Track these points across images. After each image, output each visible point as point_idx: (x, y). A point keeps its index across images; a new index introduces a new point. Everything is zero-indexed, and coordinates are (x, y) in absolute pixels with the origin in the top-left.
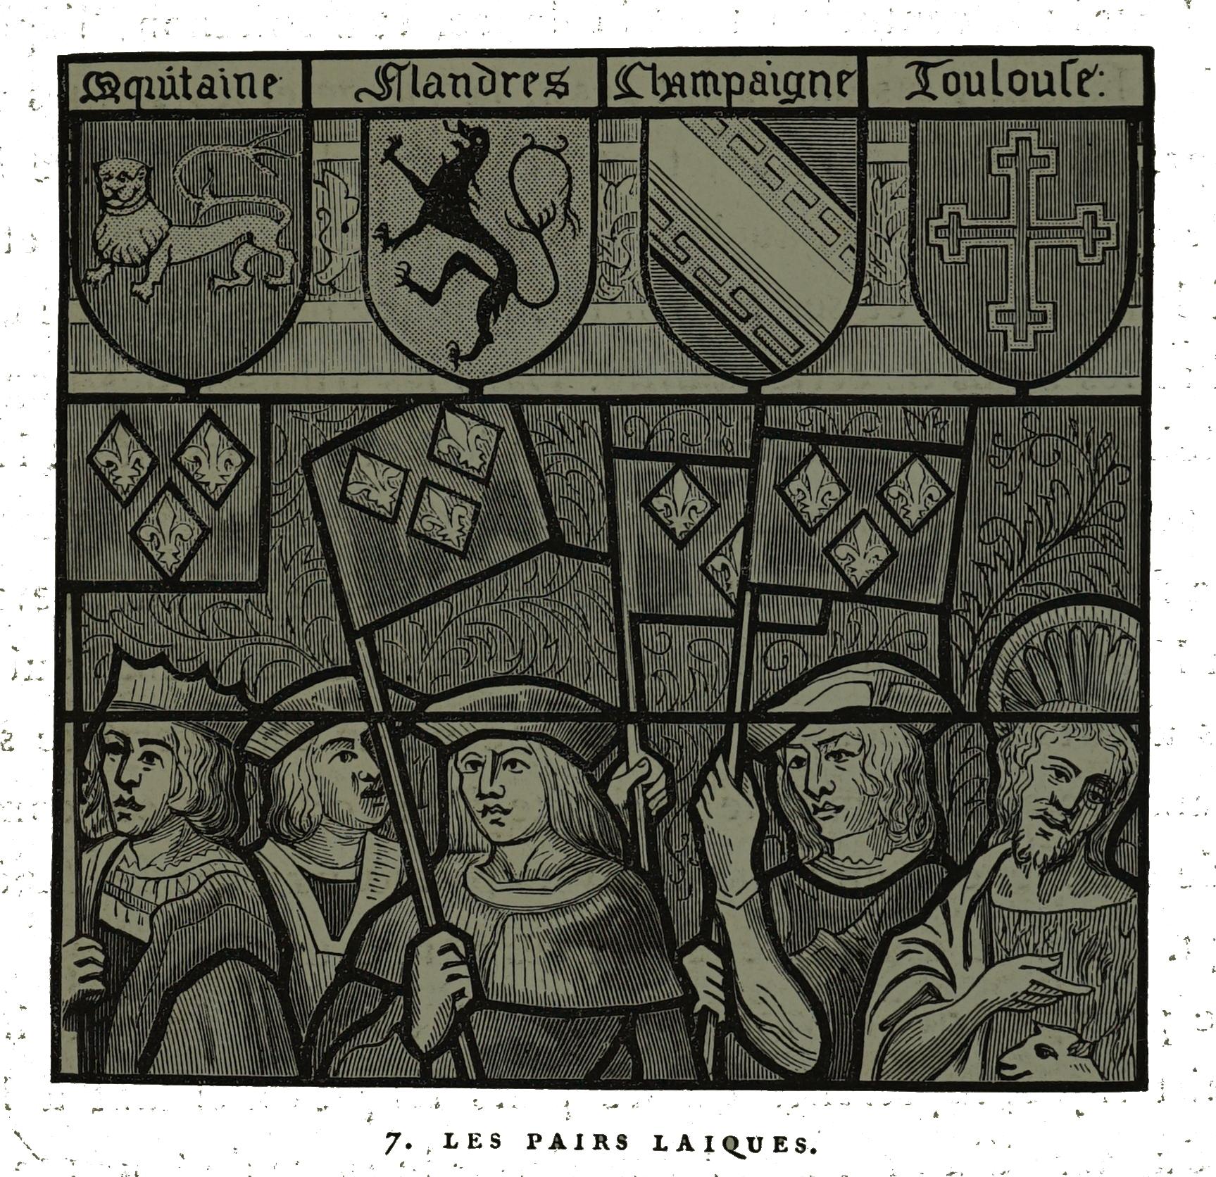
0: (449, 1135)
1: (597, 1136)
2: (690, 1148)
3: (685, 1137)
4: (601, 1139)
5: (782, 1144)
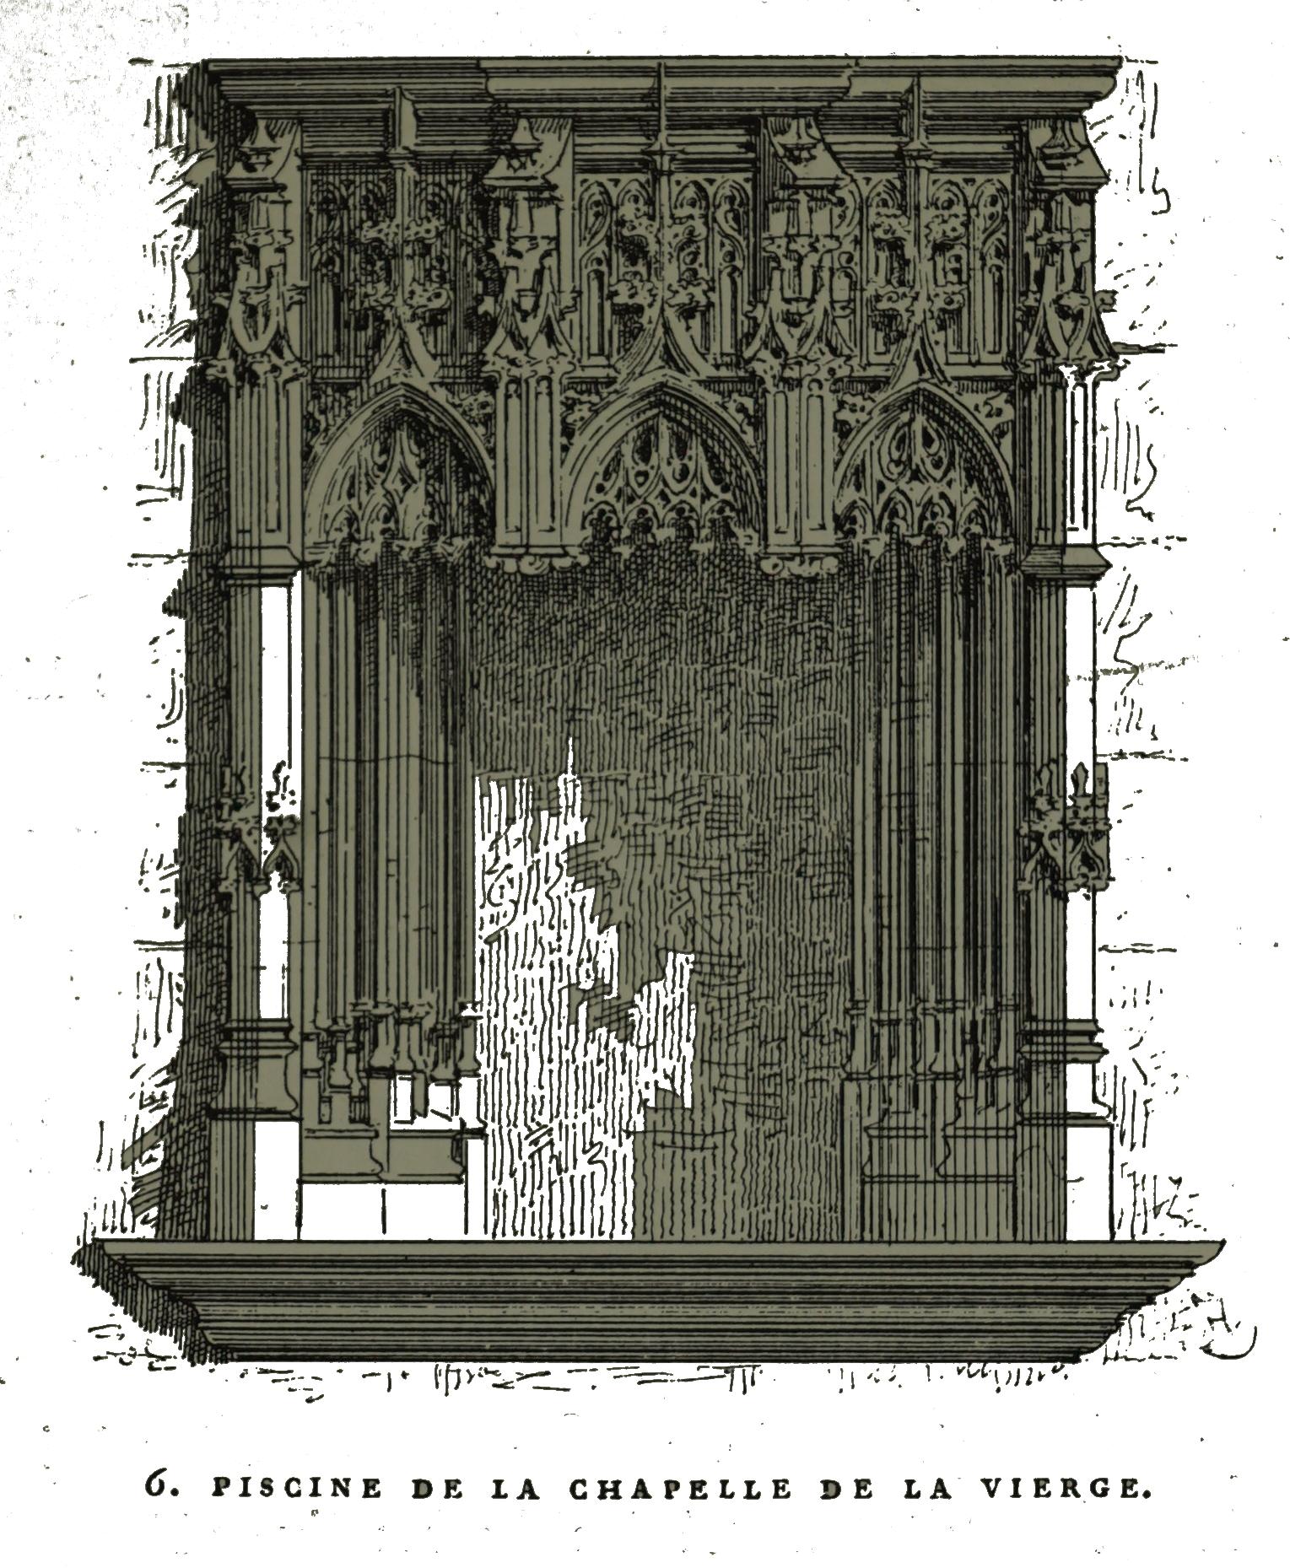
0: (910, 1483)
1: (1064, 1481)
2: (647, 1496)
3: (940, 1482)
4: (1070, 1484)
5: (783, 1488)
